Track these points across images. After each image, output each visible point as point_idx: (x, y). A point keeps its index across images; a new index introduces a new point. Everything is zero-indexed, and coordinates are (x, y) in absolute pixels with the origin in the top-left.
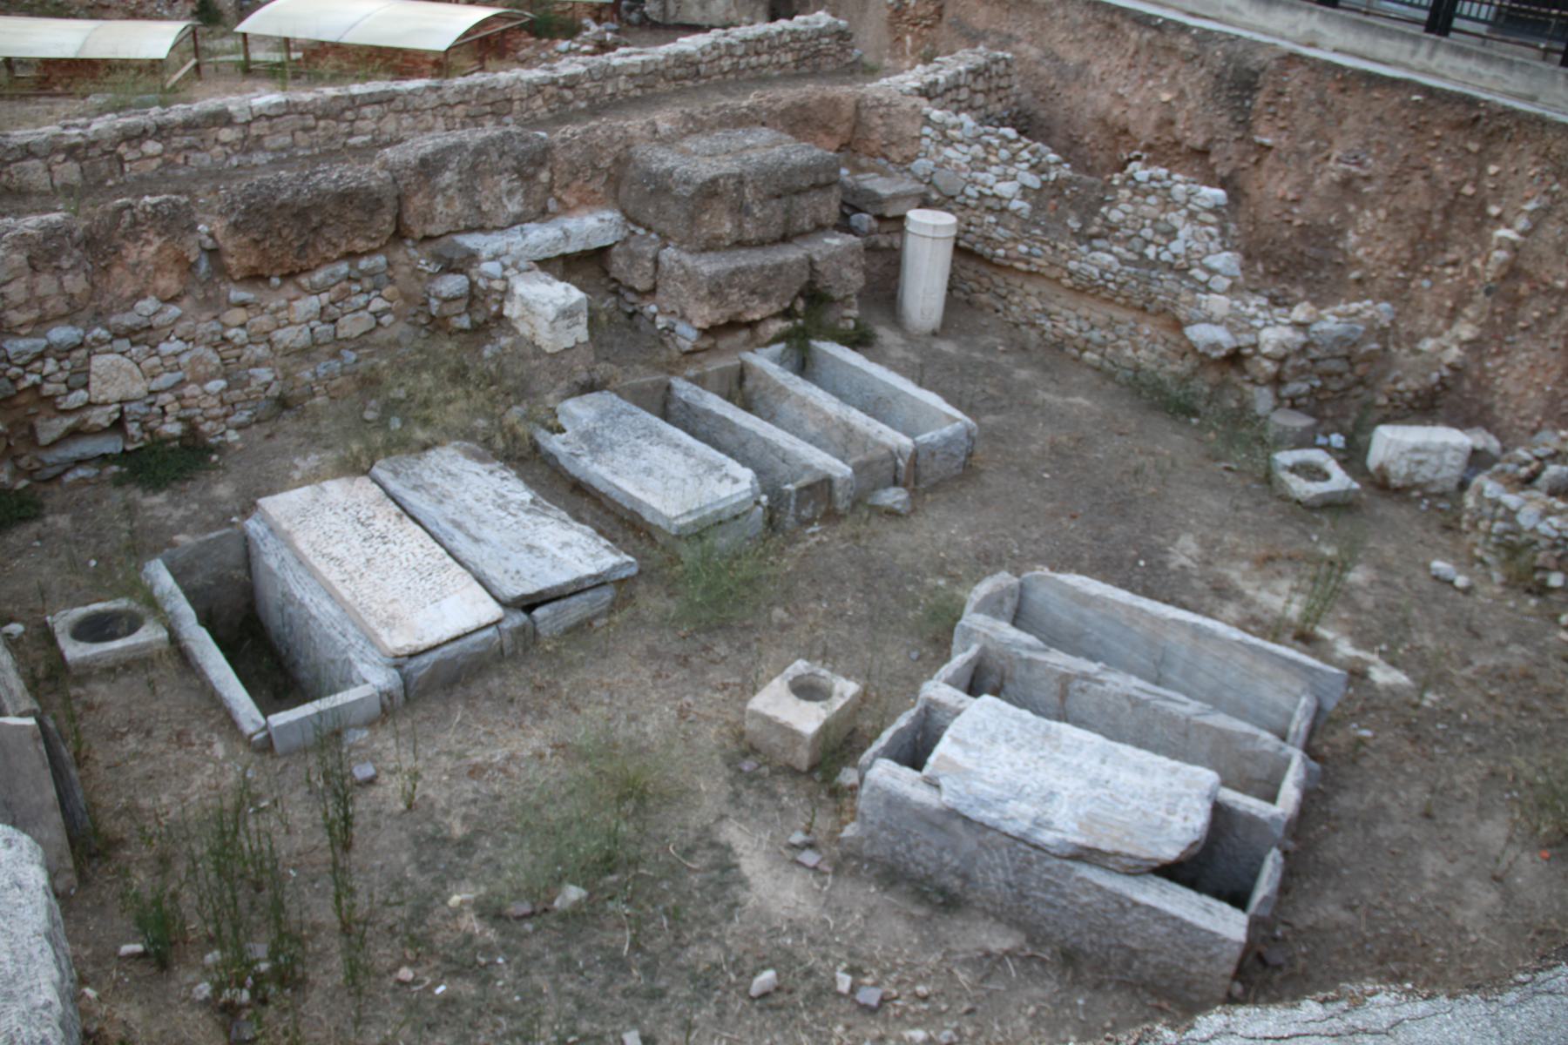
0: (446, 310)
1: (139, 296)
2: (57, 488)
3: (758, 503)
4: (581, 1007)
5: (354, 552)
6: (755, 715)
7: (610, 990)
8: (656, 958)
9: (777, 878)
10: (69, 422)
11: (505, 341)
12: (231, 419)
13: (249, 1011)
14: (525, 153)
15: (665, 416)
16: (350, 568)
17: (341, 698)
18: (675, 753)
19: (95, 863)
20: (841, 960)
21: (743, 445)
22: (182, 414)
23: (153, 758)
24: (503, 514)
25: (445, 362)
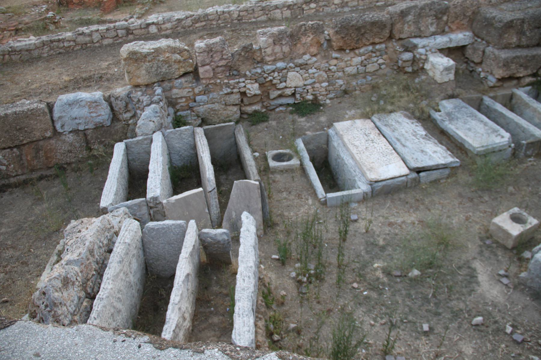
0: (404, 65)
1: (304, 54)
2: (273, 113)
3: (510, 146)
4: (410, 311)
5: (362, 144)
6: (494, 224)
7: (422, 308)
8: (440, 301)
9: (491, 285)
10: (279, 92)
11: (423, 77)
12: (328, 96)
13: (305, 284)
14: (439, 9)
15: (479, 110)
16: (360, 149)
17: (353, 191)
18: (461, 232)
19: (269, 229)
20: (509, 321)
21: (508, 124)
22: (313, 93)
23: (290, 200)
24: (415, 138)
25: (402, 83)
